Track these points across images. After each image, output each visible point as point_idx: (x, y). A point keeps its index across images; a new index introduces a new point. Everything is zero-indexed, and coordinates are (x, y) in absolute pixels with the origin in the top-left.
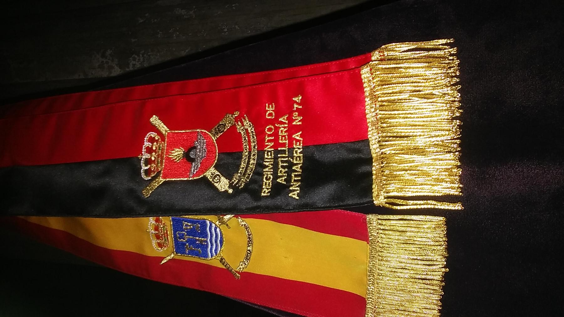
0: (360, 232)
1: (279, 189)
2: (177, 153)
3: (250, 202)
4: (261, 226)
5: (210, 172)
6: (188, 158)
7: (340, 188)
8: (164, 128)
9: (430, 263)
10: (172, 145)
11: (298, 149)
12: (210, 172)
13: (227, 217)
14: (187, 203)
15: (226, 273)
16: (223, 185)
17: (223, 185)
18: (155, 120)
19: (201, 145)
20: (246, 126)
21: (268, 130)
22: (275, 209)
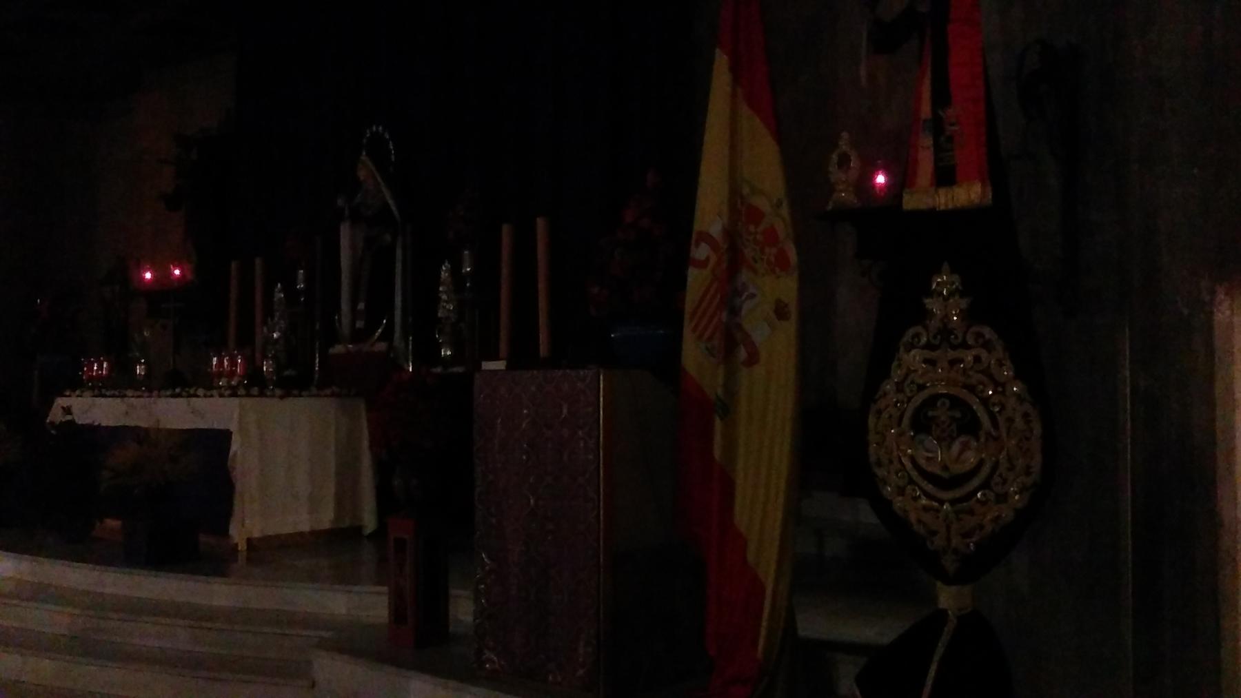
7: (945, 177)
17: (942, 139)
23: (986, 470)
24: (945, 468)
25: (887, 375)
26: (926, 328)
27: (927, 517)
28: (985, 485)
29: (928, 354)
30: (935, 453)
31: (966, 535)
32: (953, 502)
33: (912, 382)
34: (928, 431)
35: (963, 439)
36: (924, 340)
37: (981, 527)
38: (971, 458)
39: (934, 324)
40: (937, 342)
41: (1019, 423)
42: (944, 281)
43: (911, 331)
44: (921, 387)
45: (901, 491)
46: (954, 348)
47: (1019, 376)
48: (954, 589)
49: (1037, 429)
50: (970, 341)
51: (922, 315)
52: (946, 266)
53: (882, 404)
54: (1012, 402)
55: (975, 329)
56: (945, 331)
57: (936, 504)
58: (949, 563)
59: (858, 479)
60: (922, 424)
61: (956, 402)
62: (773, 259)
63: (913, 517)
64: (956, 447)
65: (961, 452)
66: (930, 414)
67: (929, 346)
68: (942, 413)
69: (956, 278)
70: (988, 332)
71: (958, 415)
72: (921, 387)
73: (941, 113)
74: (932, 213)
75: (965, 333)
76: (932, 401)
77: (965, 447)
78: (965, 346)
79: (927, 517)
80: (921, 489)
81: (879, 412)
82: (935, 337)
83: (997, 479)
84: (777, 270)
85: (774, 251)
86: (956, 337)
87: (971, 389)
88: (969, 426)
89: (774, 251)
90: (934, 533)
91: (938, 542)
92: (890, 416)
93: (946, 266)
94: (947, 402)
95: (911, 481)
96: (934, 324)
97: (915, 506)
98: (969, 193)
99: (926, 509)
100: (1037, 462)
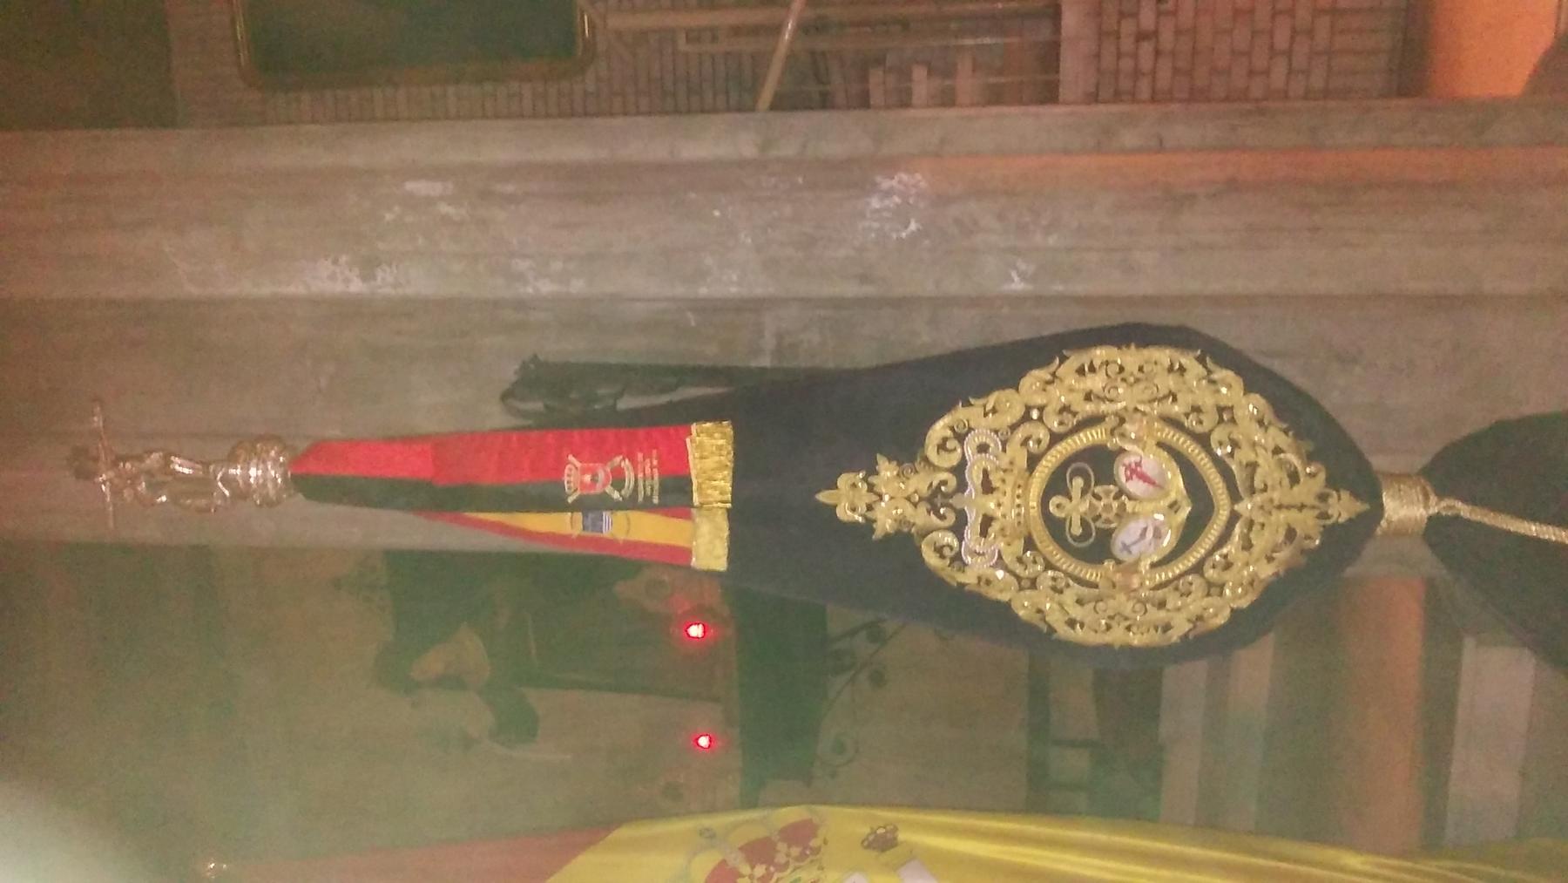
0: (687, 516)
1: (648, 498)
2: (588, 478)
3: (631, 504)
4: (635, 515)
5: (609, 489)
6: (594, 480)
7: (676, 495)
8: (578, 464)
9: (700, 446)
10: (584, 472)
11: (656, 478)
12: (609, 489)
13: (1221, 374)
14: (592, 506)
15: (611, 543)
16: (616, 495)
17: (616, 495)
18: (571, 458)
19: (601, 475)
20: (626, 464)
21: (640, 467)
22: (647, 506)
23: (1170, 435)
24: (1174, 506)
25: (1004, 610)
26: (925, 533)
27: (1260, 541)
28: (1203, 440)
29: (971, 532)
30: (1149, 521)
31: (1294, 478)
32: (1235, 497)
33: (1020, 560)
34: (1106, 536)
35: (1121, 473)
36: (949, 538)
37: (1277, 451)
38: (1153, 461)
39: (921, 517)
40: (951, 519)
41: (1096, 382)
42: (846, 498)
43: (931, 558)
44: (1029, 544)
45: (1213, 588)
46: (962, 486)
47: (1012, 382)
48: (1386, 499)
49: (1100, 354)
50: (954, 459)
51: (905, 542)
52: (823, 497)
53: (1056, 620)
54: (1058, 395)
55: (931, 452)
56: (934, 499)
57: (1237, 530)
58: (1343, 508)
59: (1131, 684)
60: (1096, 545)
61: (1056, 485)
62: (795, 851)
63: (1266, 571)
64: (1135, 487)
65: (1144, 478)
66: (1077, 530)
67: (958, 529)
68: (1074, 508)
69: (844, 481)
70: (940, 429)
71: (1078, 482)
72: (1029, 544)
73: (570, 500)
74: (736, 516)
75: (936, 469)
76: (1056, 527)
77: (1135, 472)
78: (959, 470)
79: (1260, 541)
80: (1210, 553)
81: (1072, 623)
82: (942, 517)
83: (1191, 422)
84: (814, 843)
85: (782, 847)
86: (944, 483)
87: (1033, 461)
88: (1099, 463)
89: (782, 847)
90: (1291, 534)
91: (1306, 522)
92: (1080, 602)
93: (823, 497)
94: (1055, 500)
95: (1198, 569)
96: (921, 517)
97: (1248, 567)
98: (710, 451)
99: (1247, 546)
100: (1164, 355)
